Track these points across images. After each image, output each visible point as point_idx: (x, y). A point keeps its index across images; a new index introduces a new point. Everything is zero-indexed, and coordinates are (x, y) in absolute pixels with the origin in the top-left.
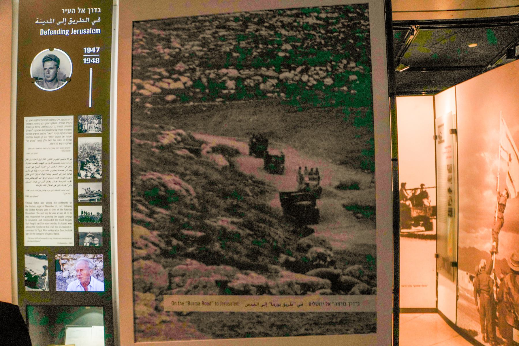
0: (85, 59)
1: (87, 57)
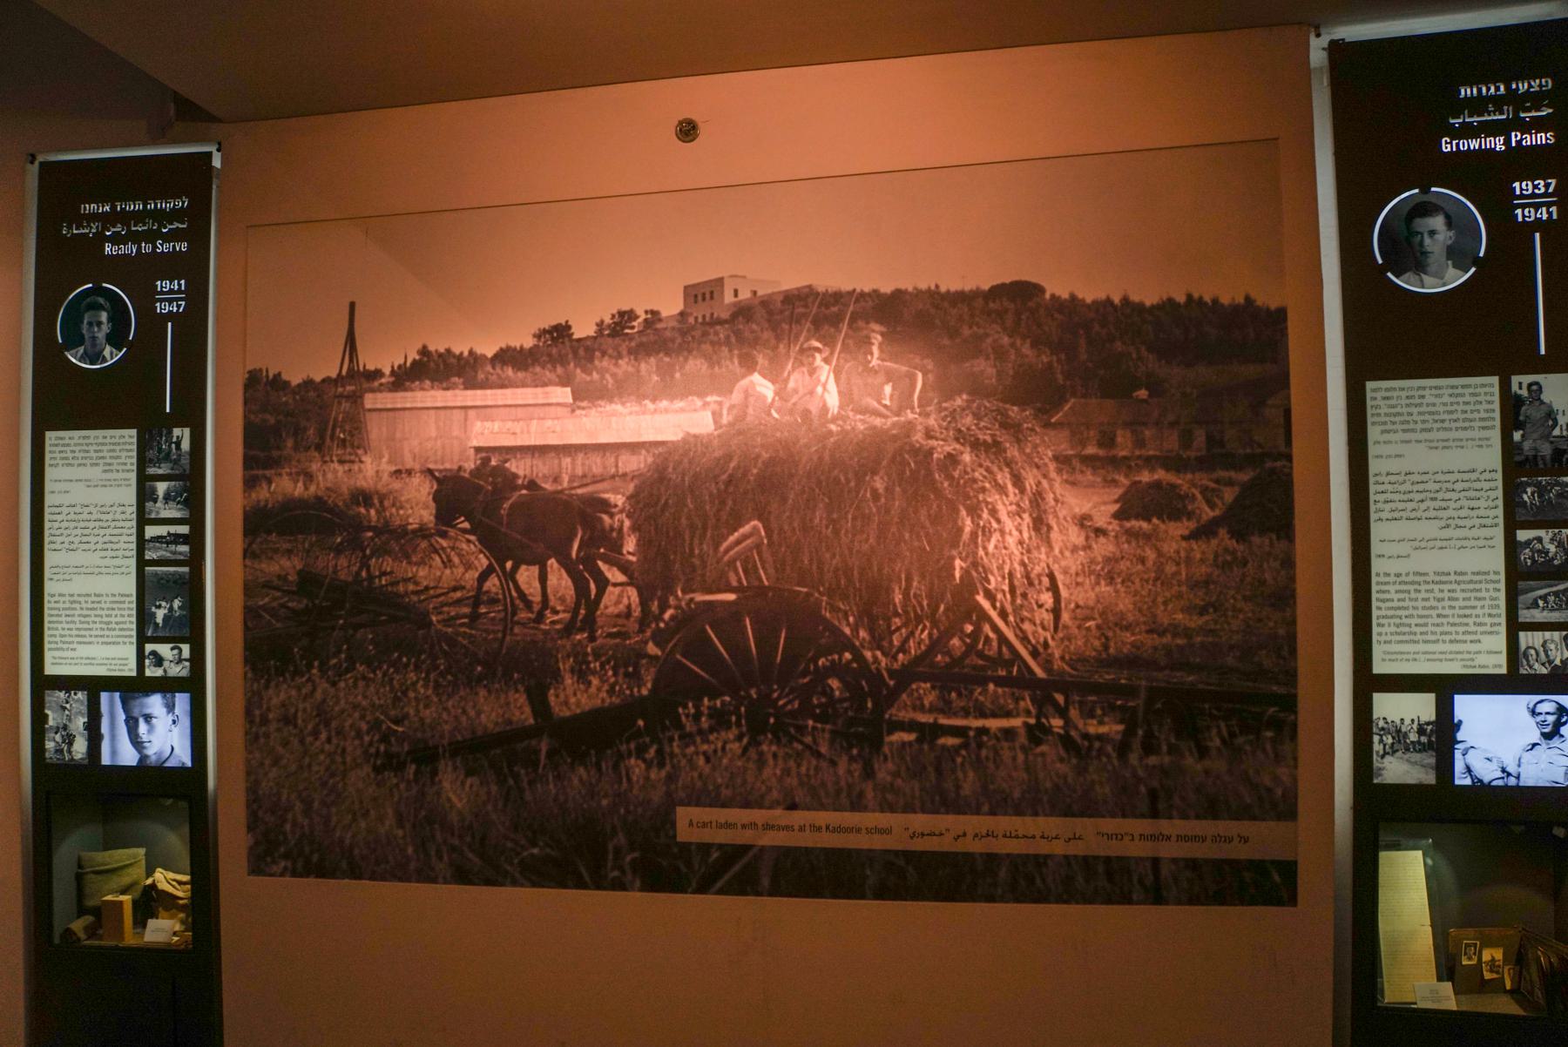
0: (1519, 211)
1: (1523, 206)
